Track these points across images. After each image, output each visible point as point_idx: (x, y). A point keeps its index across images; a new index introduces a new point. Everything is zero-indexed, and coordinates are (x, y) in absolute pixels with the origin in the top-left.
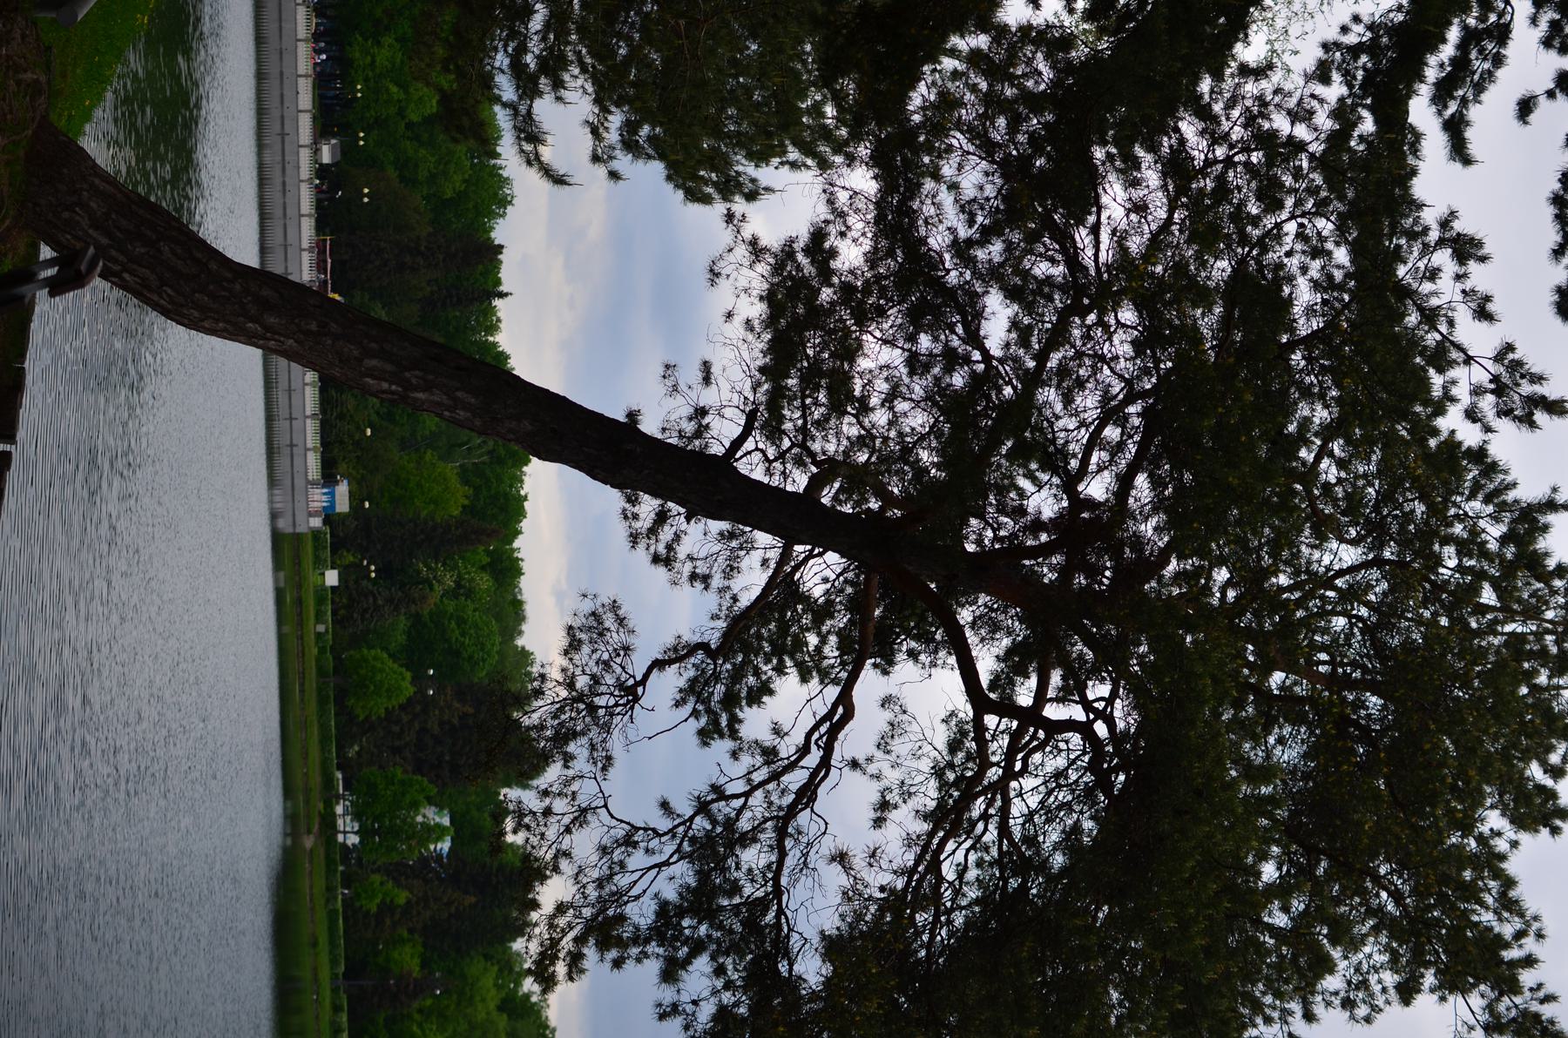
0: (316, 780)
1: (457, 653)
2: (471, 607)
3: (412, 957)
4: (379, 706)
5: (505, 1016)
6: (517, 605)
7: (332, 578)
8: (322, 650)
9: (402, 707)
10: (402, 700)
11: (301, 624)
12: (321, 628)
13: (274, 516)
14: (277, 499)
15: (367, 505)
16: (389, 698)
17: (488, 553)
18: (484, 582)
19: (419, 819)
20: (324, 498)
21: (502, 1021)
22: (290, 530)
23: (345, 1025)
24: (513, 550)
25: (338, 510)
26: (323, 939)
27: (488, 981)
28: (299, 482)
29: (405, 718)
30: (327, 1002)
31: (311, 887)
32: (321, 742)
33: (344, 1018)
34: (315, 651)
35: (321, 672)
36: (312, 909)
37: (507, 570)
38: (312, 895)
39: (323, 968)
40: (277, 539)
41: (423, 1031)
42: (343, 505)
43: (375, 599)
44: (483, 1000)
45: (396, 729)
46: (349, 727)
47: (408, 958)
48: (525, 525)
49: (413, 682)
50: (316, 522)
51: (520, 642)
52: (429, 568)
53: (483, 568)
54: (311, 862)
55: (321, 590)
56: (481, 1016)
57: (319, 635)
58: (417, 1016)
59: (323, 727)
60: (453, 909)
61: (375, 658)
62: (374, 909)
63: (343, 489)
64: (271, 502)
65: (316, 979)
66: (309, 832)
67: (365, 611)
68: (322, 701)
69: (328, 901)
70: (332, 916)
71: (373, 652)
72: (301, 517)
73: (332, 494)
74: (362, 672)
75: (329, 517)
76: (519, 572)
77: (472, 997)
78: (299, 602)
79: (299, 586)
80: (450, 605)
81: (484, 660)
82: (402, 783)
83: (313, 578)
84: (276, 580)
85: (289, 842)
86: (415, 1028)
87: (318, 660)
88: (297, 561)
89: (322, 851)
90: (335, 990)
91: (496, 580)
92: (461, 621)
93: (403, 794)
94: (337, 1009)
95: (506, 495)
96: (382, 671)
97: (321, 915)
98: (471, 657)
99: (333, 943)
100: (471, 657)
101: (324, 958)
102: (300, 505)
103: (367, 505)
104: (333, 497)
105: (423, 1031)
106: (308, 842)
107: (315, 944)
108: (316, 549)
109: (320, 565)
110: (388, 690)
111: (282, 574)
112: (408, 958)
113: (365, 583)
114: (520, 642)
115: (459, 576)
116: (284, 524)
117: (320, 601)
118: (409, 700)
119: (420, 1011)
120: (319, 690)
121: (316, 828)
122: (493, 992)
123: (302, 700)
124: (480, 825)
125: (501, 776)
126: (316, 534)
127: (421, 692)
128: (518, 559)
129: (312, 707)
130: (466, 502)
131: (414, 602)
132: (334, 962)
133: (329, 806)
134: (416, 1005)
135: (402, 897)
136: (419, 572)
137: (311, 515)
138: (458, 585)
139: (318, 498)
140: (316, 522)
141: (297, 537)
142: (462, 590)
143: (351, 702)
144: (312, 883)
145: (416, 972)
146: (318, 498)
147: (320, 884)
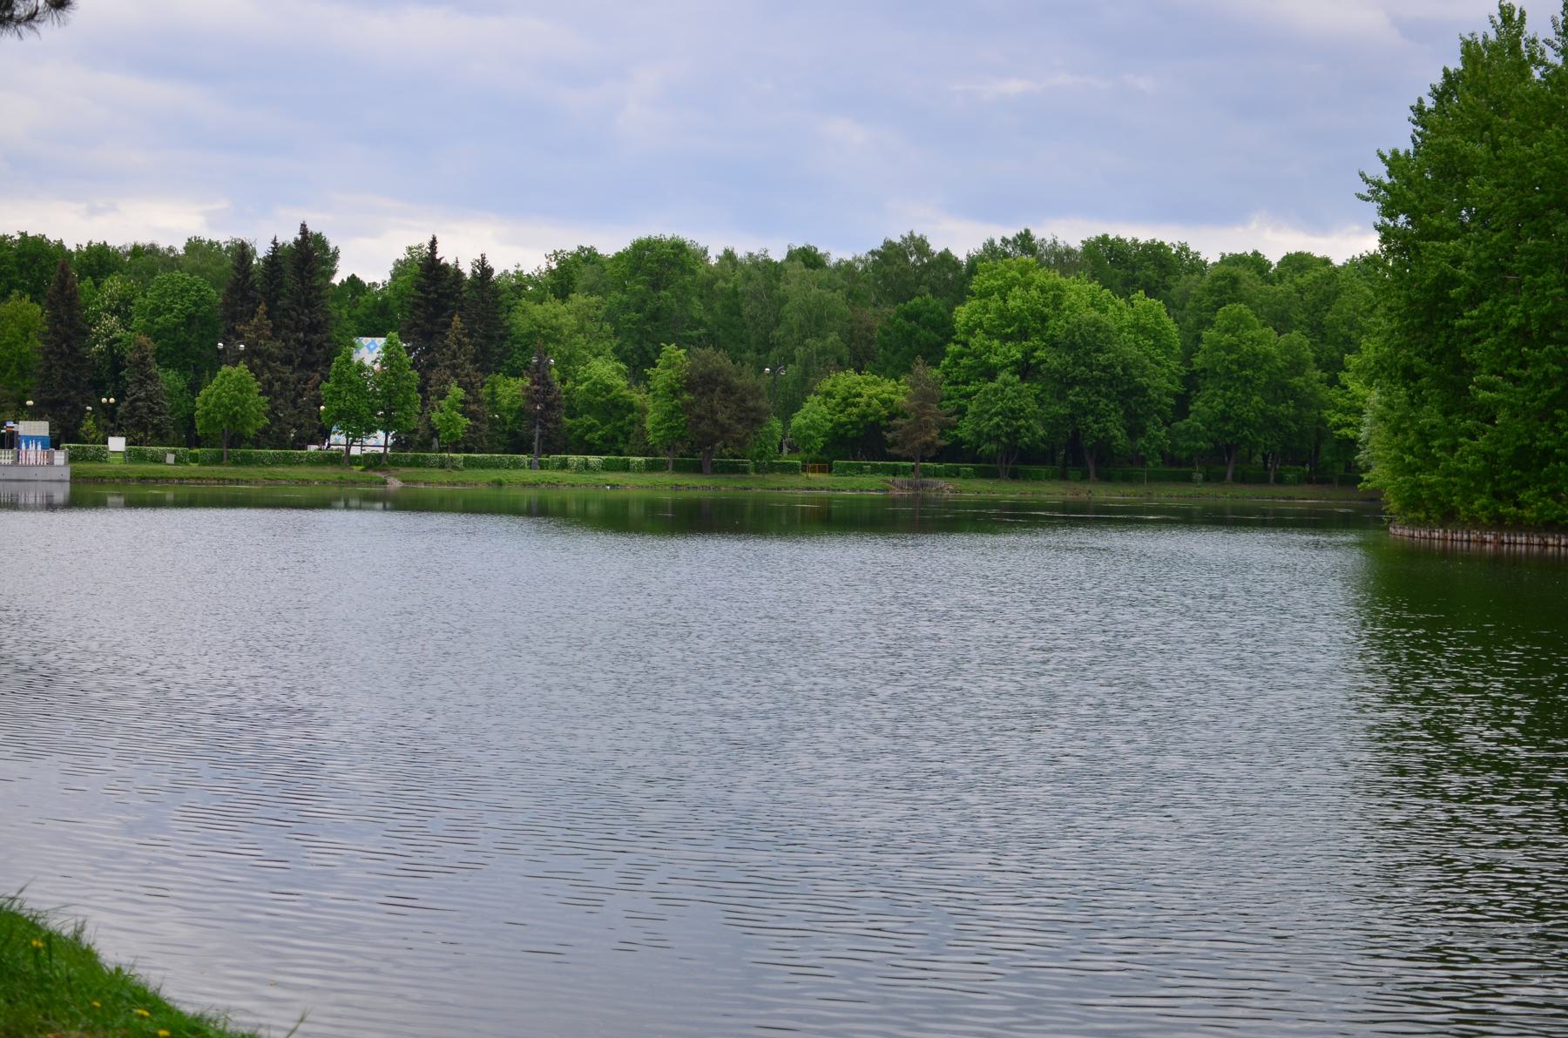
0: (330, 472)
1: (191, 317)
2: (141, 299)
3: (507, 385)
4: (257, 402)
5: (572, 296)
6: (137, 251)
7: (117, 444)
8: (195, 459)
9: (257, 377)
10: (251, 377)
11: (165, 480)
12: (170, 458)
13: (51, 506)
14: (31, 500)
15: (30, 403)
16: (249, 390)
17: (82, 278)
18: (114, 285)
19: (377, 367)
20: (32, 447)
21: (578, 299)
22: (68, 485)
23: (581, 458)
24: (79, 251)
25: (46, 433)
26: (494, 475)
27: (537, 311)
28: (15, 473)
29: (267, 375)
30: (559, 474)
31: (441, 484)
32: (290, 465)
33: (574, 459)
34: (194, 466)
35: (218, 460)
36: (464, 484)
37: (100, 260)
38: (449, 483)
39: (525, 475)
40: (75, 502)
41: (586, 379)
42: (41, 428)
43: (138, 399)
44: (556, 316)
45: (277, 386)
46: (272, 437)
47: (511, 390)
48: (52, 237)
49: (235, 364)
50: (60, 457)
51: (181, 251)
52: (97, 341)
53: (97, 285)
54: (415, 482)
55: (132, 456)
56: (572, 320)
57: (178, 461)
58: (569, 384)
59: (275, 462)
60: (466, 340)
61: (205, 404)
62: (467, 421)
63: (25, 428)
64: (34, 508)
65: (535, 485)
66: (384, 483)
67: (151, 410)
68: (247, 461)
69: (455, 468)
70: (469, 464)
71: (198, 405)
72: (54, 474)
73: (28, 439)
74: (219, 417)
75: (54, 443)
76: (103, 248)
77: (552, 328)
78: (143, 480)
79: (126, 479)
80: (138, 321)
81: (199, 290)
82: (338, 382)
83: (116, 464)
84: (116, 506)
85: (379, 505)
86: (581, 388)
87: (204, 463)
88: (100, 480)
89: (403, 470)
90: (543, 466)
91: (110, 272)
92: (157, 311)
93: (351, 382)
94: (564, 465)
95: (19, 255)
96: (219, 397)
97: (470, 475)
98: (195, 304)
99: (497, 466)
100: (195, 304)
101: (514, 475)
102: (40, 474)
103: (30, 403)
104: (32, 438)
105: (586, 379)
106: (395, 484)
107: (500, 484)
108: (85, 459)
109: (100, 457)
110: (241, 391)
111: (110, 500)
112: (511, 390)
113: (120, 410)
114: (181, 251)
115: (106, 310)
116: (60, 494)
117: (141, 458)
118: (252, 370)
119: (563, 381)
120: (236, 463)
121: (380, 475)
122: (547, 305)
123: (247, 482)
124: (373, 310)
125: (322, 280)
126: (72, 458)
127: (241, 355)
128: (89, 247)
129: (253, 471)
130: (28, 297)
131: (144, 358)
132: (517, 465)
133: (354, 461)
134: (558, 385)
135: (456, 392)
136: (100, 353)
137: (51, 463)
138: (115, 312)
139: (33, 454)
140: (60, 457)
141: (75, 479)
142: (122, 308)
143: (251, 431)
144: (434, 481)
145: (525, 382)
146: (33, 454)
147: (437, 474)
